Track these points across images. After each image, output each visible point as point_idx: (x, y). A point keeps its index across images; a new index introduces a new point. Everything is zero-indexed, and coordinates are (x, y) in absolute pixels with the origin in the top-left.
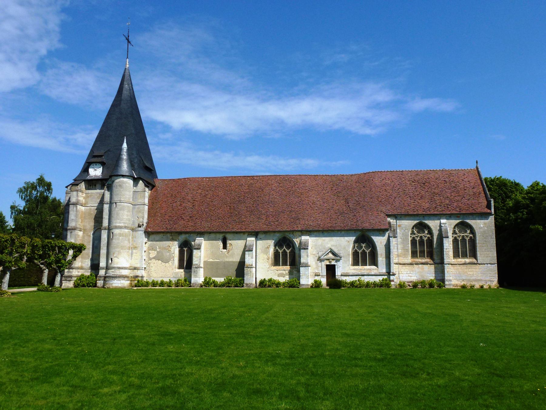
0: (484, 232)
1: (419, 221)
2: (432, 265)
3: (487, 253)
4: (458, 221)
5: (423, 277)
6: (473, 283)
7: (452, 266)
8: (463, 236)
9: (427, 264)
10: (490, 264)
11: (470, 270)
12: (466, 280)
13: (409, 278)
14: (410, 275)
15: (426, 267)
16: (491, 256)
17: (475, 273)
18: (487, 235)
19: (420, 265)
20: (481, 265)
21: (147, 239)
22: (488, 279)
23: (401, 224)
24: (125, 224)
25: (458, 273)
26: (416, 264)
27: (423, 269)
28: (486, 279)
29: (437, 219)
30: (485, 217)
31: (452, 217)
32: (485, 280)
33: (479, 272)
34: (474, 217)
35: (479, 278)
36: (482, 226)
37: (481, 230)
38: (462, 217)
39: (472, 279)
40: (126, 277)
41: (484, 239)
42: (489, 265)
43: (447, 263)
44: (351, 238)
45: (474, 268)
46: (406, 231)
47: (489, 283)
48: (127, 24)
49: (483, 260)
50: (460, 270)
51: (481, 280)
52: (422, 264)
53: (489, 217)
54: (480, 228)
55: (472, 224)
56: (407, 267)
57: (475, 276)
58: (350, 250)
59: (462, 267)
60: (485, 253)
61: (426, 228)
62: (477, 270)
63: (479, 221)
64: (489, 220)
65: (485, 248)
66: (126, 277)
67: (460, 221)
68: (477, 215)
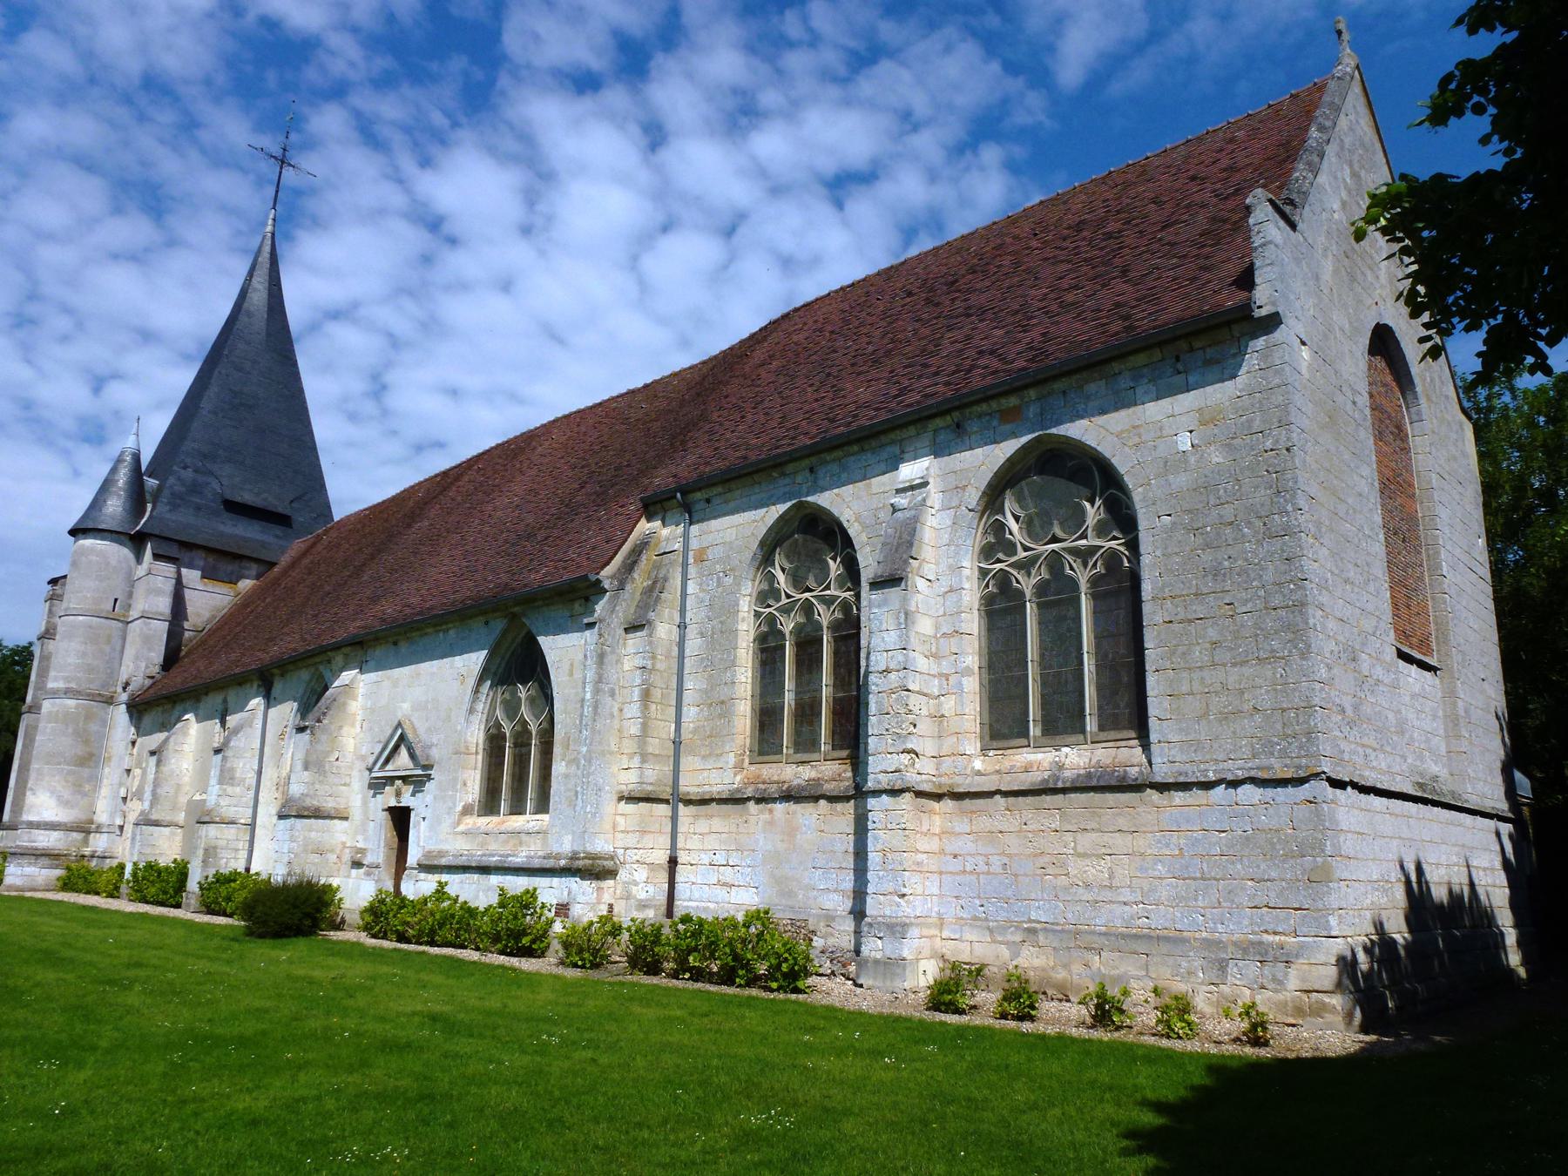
0: (1206, 487)
1: (789, 504)
2: (839, 806)
3: (1233, 677)
4: (1009, 447)
5: (790, 894)
6: (1108, 967)
7: (963, 812)
8: (1055, 560)
9: (816, 799)
10: (1355, 785)
11: (1086, 841)
12: (1049, 929)
13: (721, 893)
14: (728, 874)
15: (807, 816)
16: (1266, 702)
17: (1122, 875)
18: (1228, 512)
19: (779, 807)
20: (1179, 797)
21: (133, 730)
22: (1238, 928)
23: (707, 540)
24: (69, 682)
25: (996, 862)
26: (759, 801)
27: (791, 831)
28: (1222, 932)
29: (883, 466)
30: (1208, 363)
31: (973, 426)
32: (1209, 944)
33: (1158, 858)
34: (1124, 382)
35: (1160, 919)
36: (1184, 442)
37: (1181, 480)
38: (1032, 411)
39: (1100, 921)
40: (42, 855)
41: (1207, 557)
42: (1248, 793)
43: (885, 781)
44: (473, 656)
45: (1122, 823)
46: (728, 581)
47: (1242, 984)
48: (1475, 273)
49: (1197, 745)
50: (1014, 844)
51: (1173, 941)
52: (791, 796)
53: (1241, 353)
54: (1175, 462)
55: (1091, 441)
56: (717, 823)
57: (1127, 895)
58: (476, 735)
59: (1028, 815)
60: (1213, 677)
61: (833, 547)
62: (1141, 842)
63: (1154, 411)
64: (1242, 379)
65: (1212, 633)
66: (42, 855)
67: (1024, 439)
68: (1141, 359)
